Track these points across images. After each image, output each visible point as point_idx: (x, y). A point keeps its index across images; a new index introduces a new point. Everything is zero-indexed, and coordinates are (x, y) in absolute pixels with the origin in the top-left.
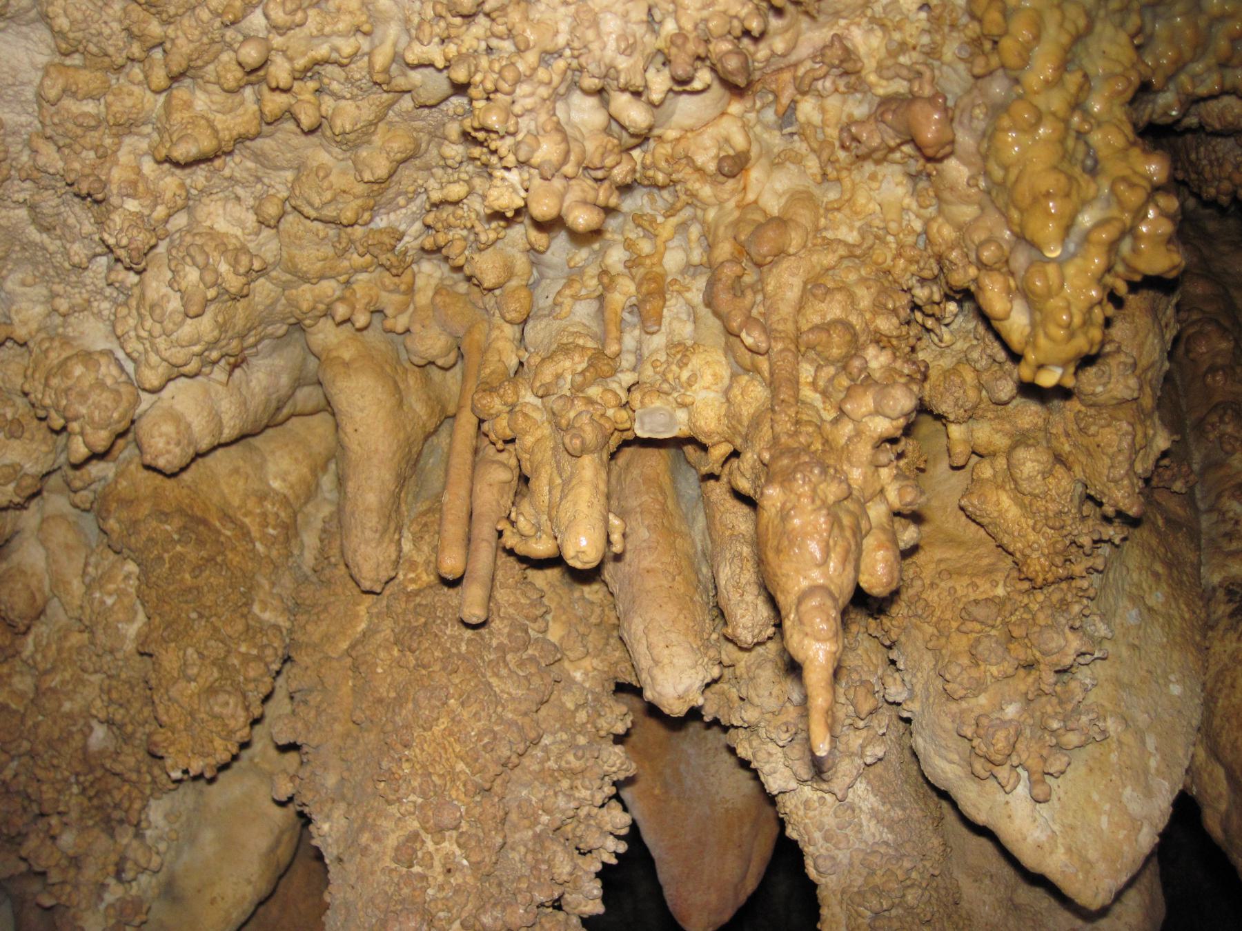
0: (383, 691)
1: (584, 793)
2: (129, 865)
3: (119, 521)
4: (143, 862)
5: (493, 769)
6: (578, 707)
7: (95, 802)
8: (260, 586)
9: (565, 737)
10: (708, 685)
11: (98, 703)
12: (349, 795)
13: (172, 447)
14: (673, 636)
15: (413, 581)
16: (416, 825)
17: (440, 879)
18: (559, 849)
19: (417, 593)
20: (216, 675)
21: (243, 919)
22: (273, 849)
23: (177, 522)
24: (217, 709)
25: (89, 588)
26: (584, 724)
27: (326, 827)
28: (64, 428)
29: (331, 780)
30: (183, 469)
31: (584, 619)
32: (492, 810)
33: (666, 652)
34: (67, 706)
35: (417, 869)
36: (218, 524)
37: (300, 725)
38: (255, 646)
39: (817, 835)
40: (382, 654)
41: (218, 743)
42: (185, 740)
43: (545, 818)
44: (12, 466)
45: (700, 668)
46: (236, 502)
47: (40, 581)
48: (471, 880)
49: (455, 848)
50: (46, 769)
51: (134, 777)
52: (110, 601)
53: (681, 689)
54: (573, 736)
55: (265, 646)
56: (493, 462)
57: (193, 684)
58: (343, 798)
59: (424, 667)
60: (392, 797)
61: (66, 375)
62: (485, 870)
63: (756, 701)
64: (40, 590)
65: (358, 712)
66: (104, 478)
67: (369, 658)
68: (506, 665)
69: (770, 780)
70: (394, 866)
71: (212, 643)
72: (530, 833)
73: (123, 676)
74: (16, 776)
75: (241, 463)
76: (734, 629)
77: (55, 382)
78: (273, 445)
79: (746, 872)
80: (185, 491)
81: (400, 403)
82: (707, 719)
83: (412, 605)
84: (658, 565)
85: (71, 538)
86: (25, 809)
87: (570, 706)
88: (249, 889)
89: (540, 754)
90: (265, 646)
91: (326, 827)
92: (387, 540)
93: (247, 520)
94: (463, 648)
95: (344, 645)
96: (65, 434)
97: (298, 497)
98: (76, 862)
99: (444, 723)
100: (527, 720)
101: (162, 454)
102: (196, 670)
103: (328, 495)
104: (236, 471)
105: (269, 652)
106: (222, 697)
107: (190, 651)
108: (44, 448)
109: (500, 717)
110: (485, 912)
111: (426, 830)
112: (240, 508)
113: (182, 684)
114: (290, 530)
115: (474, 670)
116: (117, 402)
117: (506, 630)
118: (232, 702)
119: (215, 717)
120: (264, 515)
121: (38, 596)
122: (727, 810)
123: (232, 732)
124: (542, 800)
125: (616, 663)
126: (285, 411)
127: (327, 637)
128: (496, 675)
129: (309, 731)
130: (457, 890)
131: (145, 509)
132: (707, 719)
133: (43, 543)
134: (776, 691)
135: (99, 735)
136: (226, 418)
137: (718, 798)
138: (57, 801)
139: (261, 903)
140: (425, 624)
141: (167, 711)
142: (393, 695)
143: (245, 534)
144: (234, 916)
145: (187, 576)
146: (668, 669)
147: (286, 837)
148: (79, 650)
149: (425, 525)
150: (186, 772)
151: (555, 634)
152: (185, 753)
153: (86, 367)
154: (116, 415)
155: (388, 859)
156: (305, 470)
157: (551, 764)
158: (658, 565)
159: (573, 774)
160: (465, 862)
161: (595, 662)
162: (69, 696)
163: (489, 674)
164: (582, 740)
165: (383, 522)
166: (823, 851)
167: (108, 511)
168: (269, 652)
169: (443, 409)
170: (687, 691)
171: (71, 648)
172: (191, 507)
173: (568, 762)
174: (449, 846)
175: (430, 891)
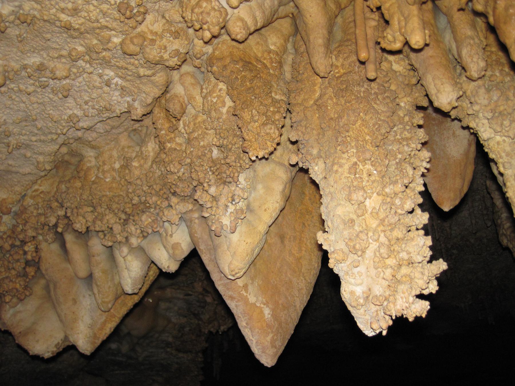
0: (332, 115)
1: (413, 146)
2: (236, 197)
3: (218, 67)
4: (242, 195)
5: (380, 137)
6: (405, 115)
7: (219, 177)
8: (273, 86)
9: (401, 127)
10: (458, 98)
11: (215, 140)
12: (324, 156)
13: (242, 30)
14: (444, 80)
15: (337, 73)
16: (355, 160)
17: (367, 179)
18: (408, 165)
19: (341, 77)
20: (265, 119)
21: (276, 217)
22: (284, 190)
23: (241, 64)
24: (268, 131)
25: (204, 98)
26: (408, 122)
27: (316, 168)
28: (201, 28)
29: (315, 152)
30: (246, 40)
31: (403, 82)
32: (383, 151)
33: (442, 86)
34: (202, 143)
35: (357, 176)
36: (255, 63)
37: (300, 133)
38: (276, 108)
39: (503, 154)
40: (329, 102)
41: (269, 143)
42: (255, 145)
43: (400, 156)
44: (176, 50)
45: (455, 92)
46: (260, 55)
47: (183, 99)
48: (377, 178)
49: (370, 167)
50: (199, 166)
51: (234, 164)
52: (215, 101)
53: (449, 100)
54: (404, 126)
55: (280, 107)
56: (370, 19)
57: (257, 123)
58: (321, 157)
59: (349, 102)
60: (345, 150)
61: (201, 7)
62: (383, 174)
63: (479, 102)
64: (184, 102)
65: (323, 124)
66: (207, 53)
67: (324, 104)
68: (379, 100)
69: (484, 134)
70: (348, 175)
71: (261, 107)
72: (395, 162)
73: (224, 128)
74: (183, 174)
75: (259, 40)
76: (470, 72)
77: (196, 10)
78: (269, 33)
79: (464, 184)
80: (241, 52)
81: (325, 4)
82: (452, 117)
83: (339, 81)
84: (435, 54)
85: (193, 81)
86: (189, 186)
87: (402, 115)
88: (278, 205)
89: (393, 134)
90: (280, 107)
91: (316, 168)
92: (328, 57)
93: (265, 61)
94: (362, 95)
95: (311, 102)
96: (201, 30)
97: (281, 52)
98: (215, 199)
99: (359, 122)
100: (389, 119)
101: (239, 34)
102: (257, 117)
103: (291, 51)
104: (258, 43)
105: (282, 109)
106: (269, 126)
107: (254, 111)
108: (186, 42)
109: (379, 119)
110: (386, 187)
111: (359, 161)
112: (262, 57)
113: (252, 124)
114: (281, 64)
115: (368, 102)
116: (221, 15)
117: (376, 87)
118: (273, 127)
119: (267, 134)
120: (271, 58)
121: (183, 104)
122: (454, 161)
123: (274, 139)
124: (398, 149)
125: (417, 98)
126: (275, 17)
127: (305, 100)
128: (375, 103)
129: (304, 135)
130: (373, 182)
131: (228, 61)
132: (452, 117)
133: (182, 84)
134: (486, 97)
135: (215, 152)
136: (258, 19)
137: (450, 156)
138: (205, 178)
139: (281, 211)
140: (347, 87)
141: (248, 135)
142: (336, 116)
143: (266, 66)
144: (273, 215)
145: (248, 84)
146: (443, 93)
147: (288, 186)
148: (204, 121)
149: (339, 51)
150: (257, 157)
151: (393, 87)
152: (256, 149)
153: (207, 3)
154: (221, 20)
155: (345, 173)
156: (282, 41)
157: (398, 137)
158: (435, 54)
159: (407, 139)
160: (375, 172)
161: (409, 99)
162: (203, 139)
163: (373, 103)
164: (408, 128)
165: (326, 50)
166: (506, 160)
167: (213, 63)
168: (282, 109)
169: (340, 6)
170: (451, 101)
171: (199, 122)
172: (244, 58)
173: (405, 135)
174: (368, 166)
175: (364, 183)
